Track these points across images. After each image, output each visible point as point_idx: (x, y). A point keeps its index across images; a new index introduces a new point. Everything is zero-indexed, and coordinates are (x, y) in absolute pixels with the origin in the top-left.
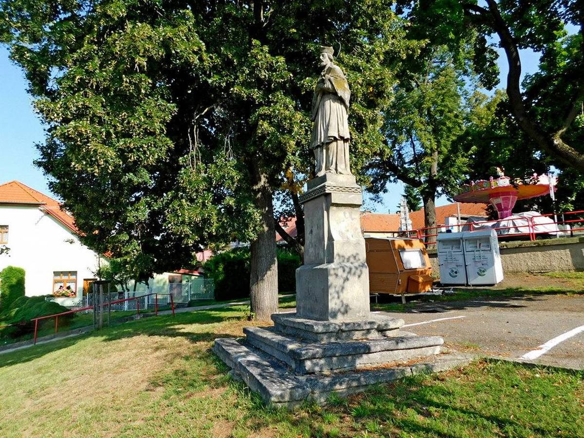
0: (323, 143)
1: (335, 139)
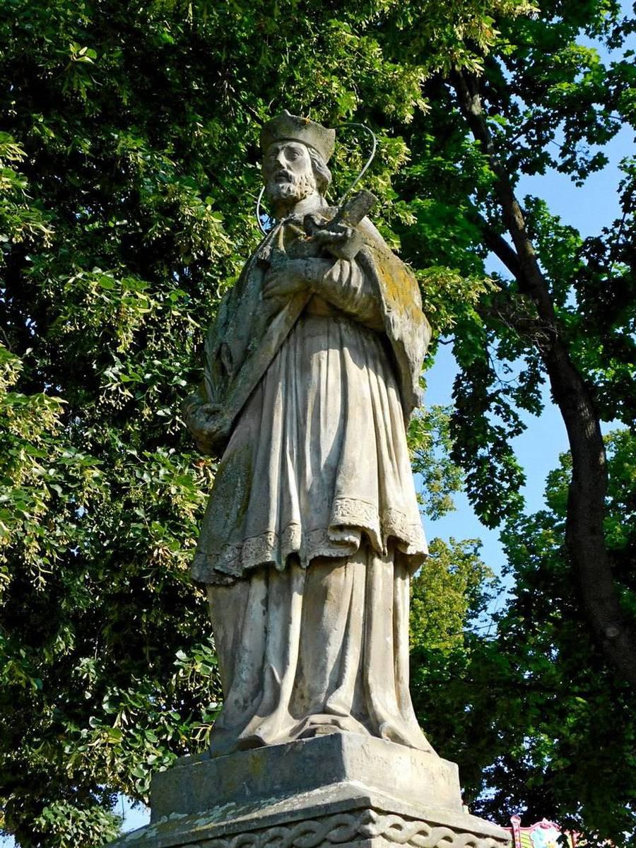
0: (294, 558)
1: (367, 550)
